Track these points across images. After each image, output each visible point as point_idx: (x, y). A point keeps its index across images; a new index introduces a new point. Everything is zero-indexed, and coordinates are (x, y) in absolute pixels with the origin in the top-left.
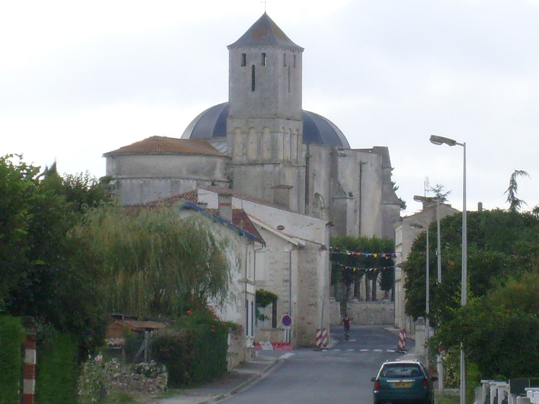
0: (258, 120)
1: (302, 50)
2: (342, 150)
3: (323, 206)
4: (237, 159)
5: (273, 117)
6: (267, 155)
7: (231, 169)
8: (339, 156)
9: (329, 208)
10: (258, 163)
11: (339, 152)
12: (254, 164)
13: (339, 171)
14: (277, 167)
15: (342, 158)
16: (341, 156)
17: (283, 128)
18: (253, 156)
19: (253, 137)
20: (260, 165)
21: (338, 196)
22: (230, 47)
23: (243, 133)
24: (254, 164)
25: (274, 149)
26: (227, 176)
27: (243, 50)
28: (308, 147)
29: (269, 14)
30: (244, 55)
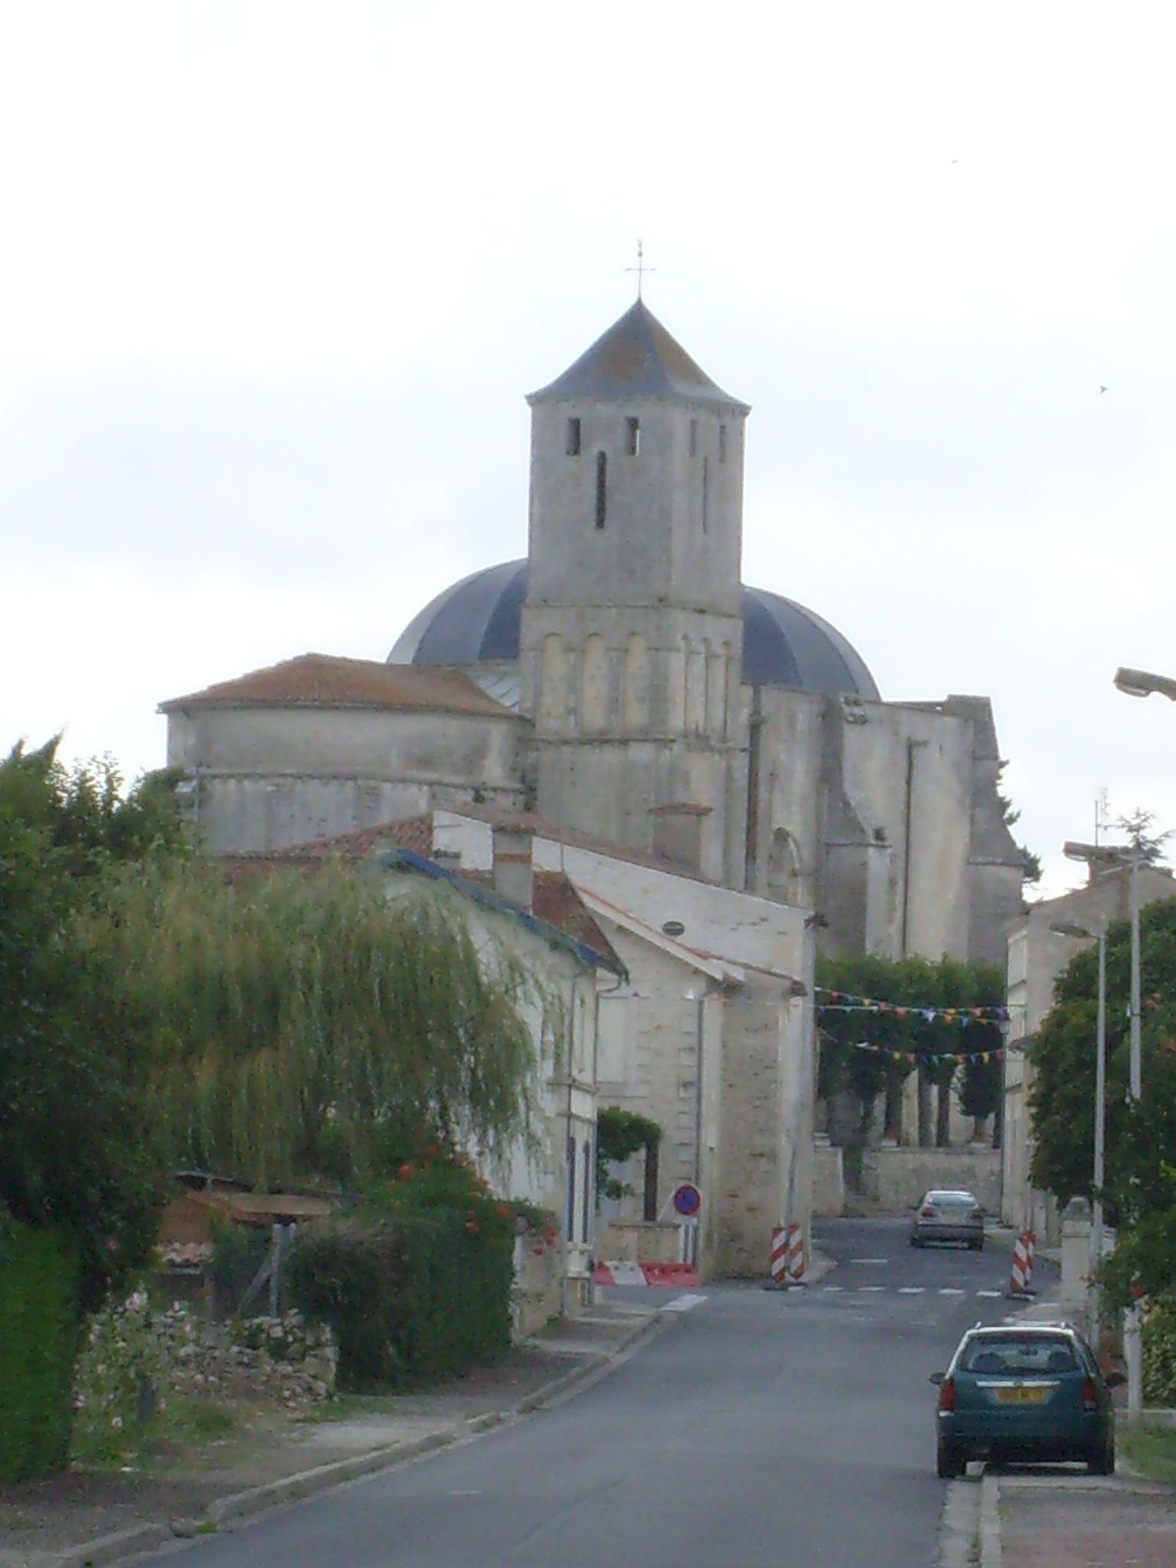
1: (743, 411)
2: (856, 703)
3: (797, 866)
4: (551, 724)
6: (636, 715)
8: (849, 722)
11: (847, 709)
12: (600, 740)
16: (855, 722)
17: (685, 637)
18: (595, 717)
19: (597, 661)
20: (616, 745)
24: (600, 740)
25: (657, 696)
26: (519, 774)
30: (576, 425)
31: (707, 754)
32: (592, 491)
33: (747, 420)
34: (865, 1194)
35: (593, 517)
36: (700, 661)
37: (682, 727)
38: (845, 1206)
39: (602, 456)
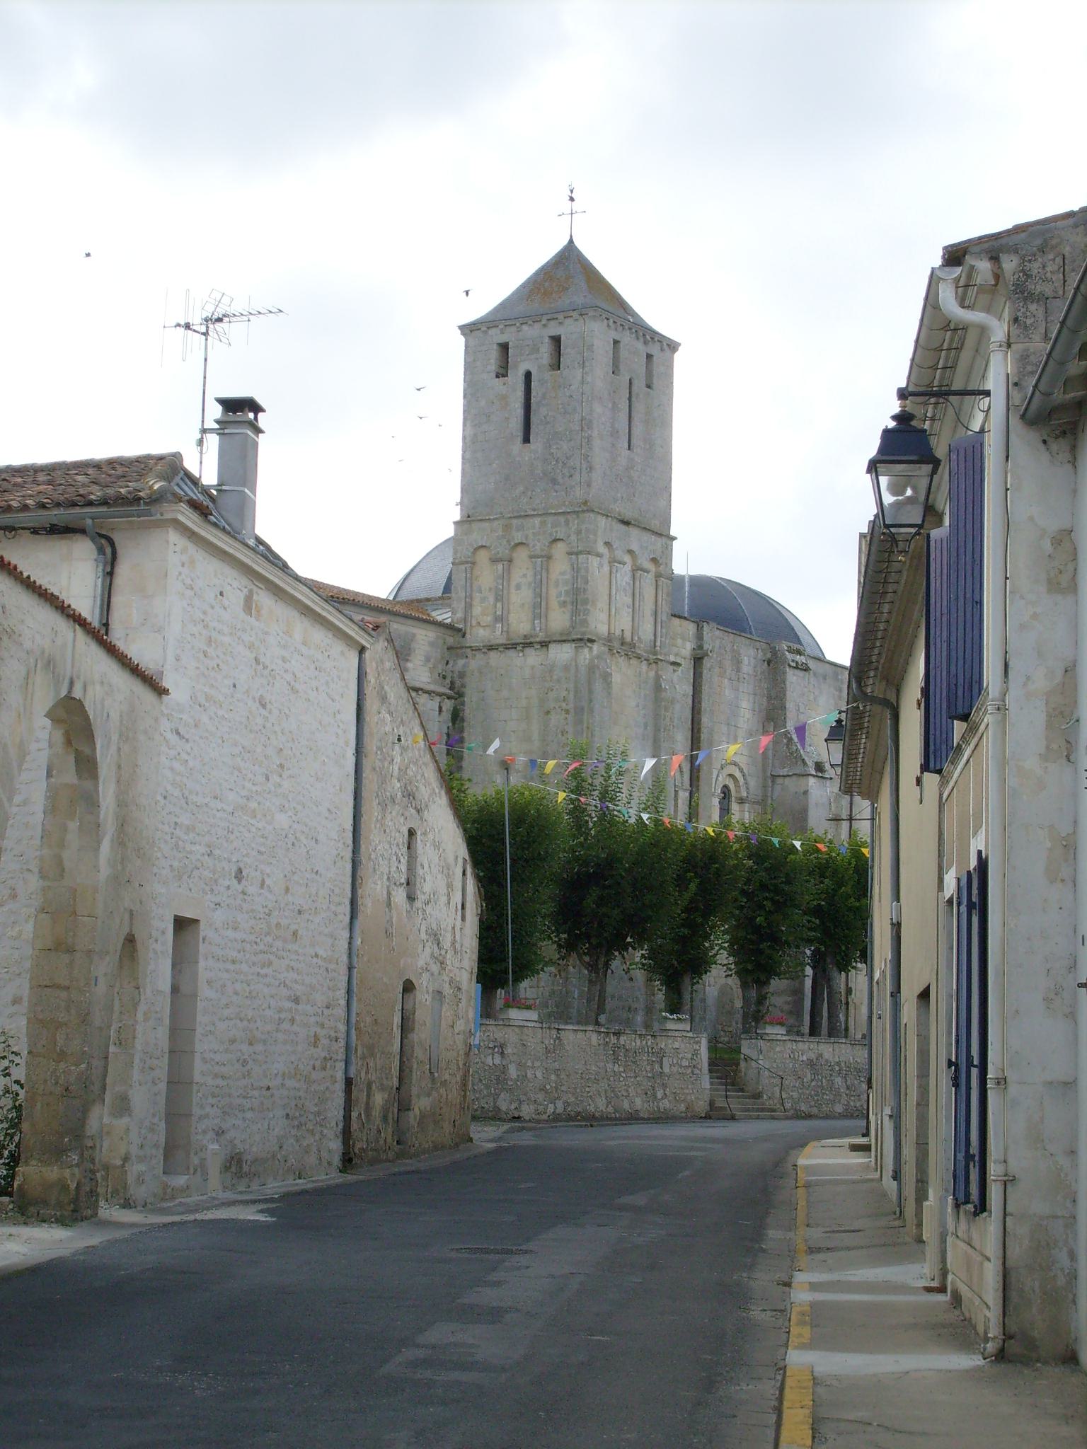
0: (537, 521)
1: (673, 346)
2: (799, 653)
3: (744, 794)
4: (479, 635)
5: (577, 509)
6: (558, 620)
7: (461, 662)
8: (790, 666)
9: (762, 802)
10: (532, 640)
11: (789, 656)
12: (526, 644)
13: (790, 705)
14: (586, 650)
15: (797, 672)
16: (796, 668)
17: (607, 544)
18: (521, 624)
19: (523, 570)
20: (538, 646)
21: (785, 772)
22: (469, 330)
23: (494, 560)
24: (526, 644)
25: (578, 600)
26: (448, 681)
27: (502, 332)
28: (699, 629)
29: (579, 244)
30: (504, 347)
31: (634, 661)
32: (520, 412)
33: (676, 356)
34: (742, 1090)
35: (520, 434)
36: (625, 571)
37: (606, 634)
38: (711, 1103)
39: (528, 376)
